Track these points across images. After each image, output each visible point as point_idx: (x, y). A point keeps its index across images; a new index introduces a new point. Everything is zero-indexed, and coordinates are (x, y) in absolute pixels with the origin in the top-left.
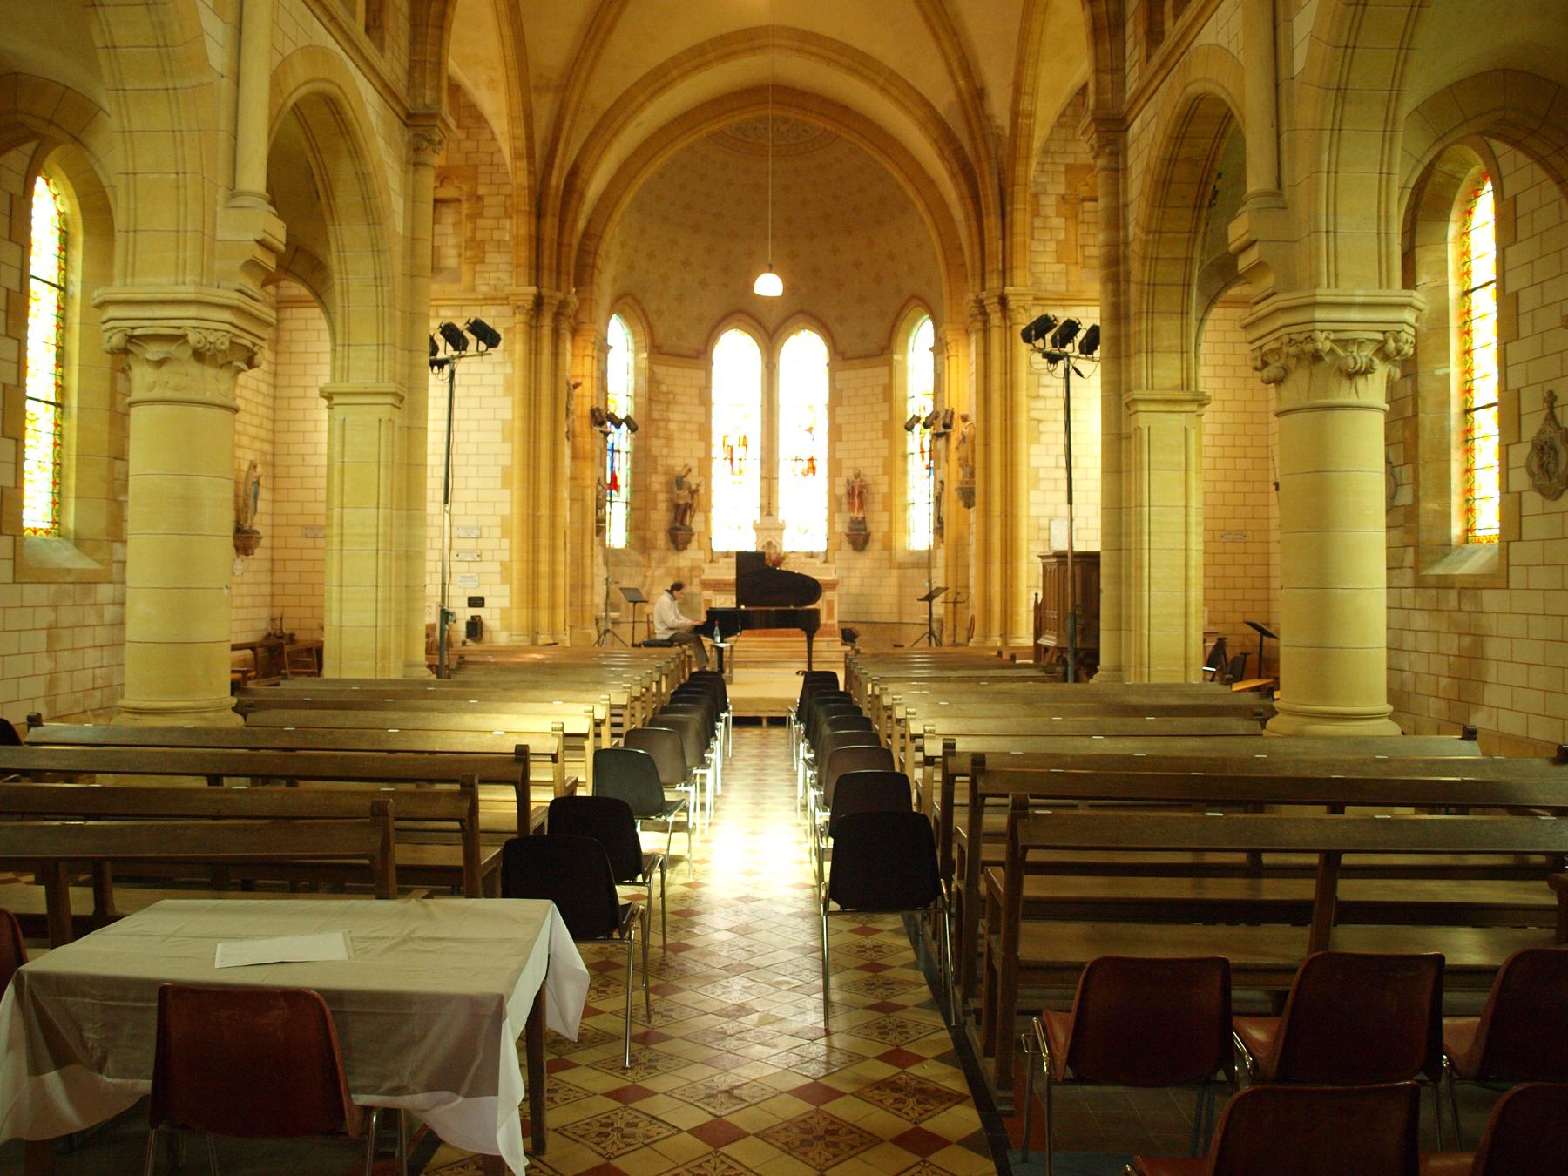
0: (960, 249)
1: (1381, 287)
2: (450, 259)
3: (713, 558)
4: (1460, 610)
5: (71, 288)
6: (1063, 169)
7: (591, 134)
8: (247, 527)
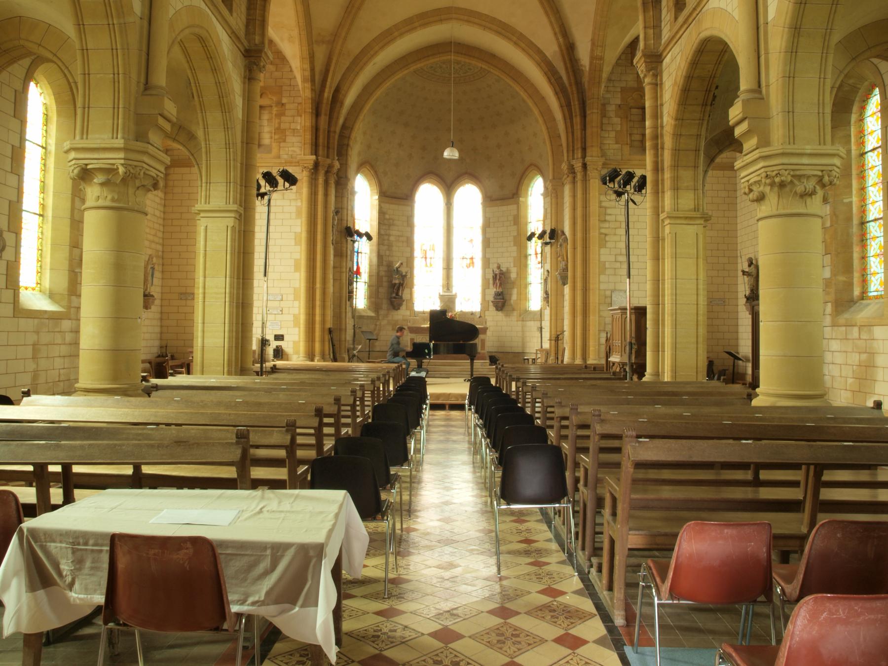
0: (559, 136)
1: (820, 144)
2: (266, 140)
3: (416, 314)
4: (860, 339)
5: (49, 148)
6: (619, 90)
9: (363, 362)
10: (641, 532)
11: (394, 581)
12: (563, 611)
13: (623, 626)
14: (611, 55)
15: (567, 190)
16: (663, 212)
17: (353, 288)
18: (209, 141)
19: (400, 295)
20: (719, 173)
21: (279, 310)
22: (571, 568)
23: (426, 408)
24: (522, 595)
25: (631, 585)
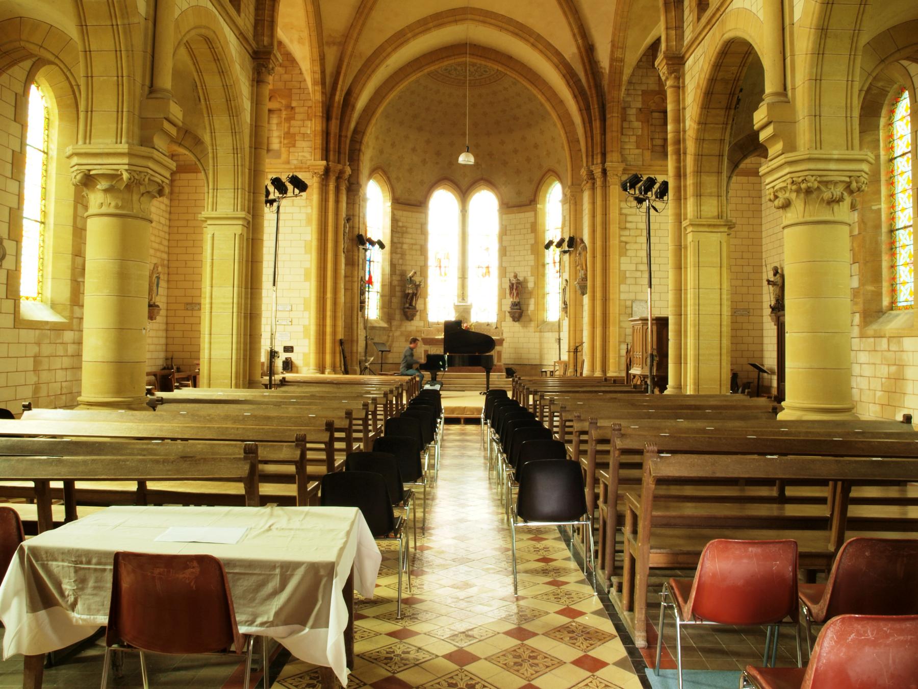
0: (578, 141)
1: (847, 149)
2: (275, 144)
4: (889, 350)
5: (50, 153)
6: (640, 93)
7: (359, 70)
10: (662, 551)
11: (407, 601)
12: (582, 632)
13: (644, 648)
14: (632, 58)
15: (586, 196)
16: (685, 219)
20: (744, 179)
21: (288, 321)
22: (590, 587)
24: (540, 616)
25: (652, 605)
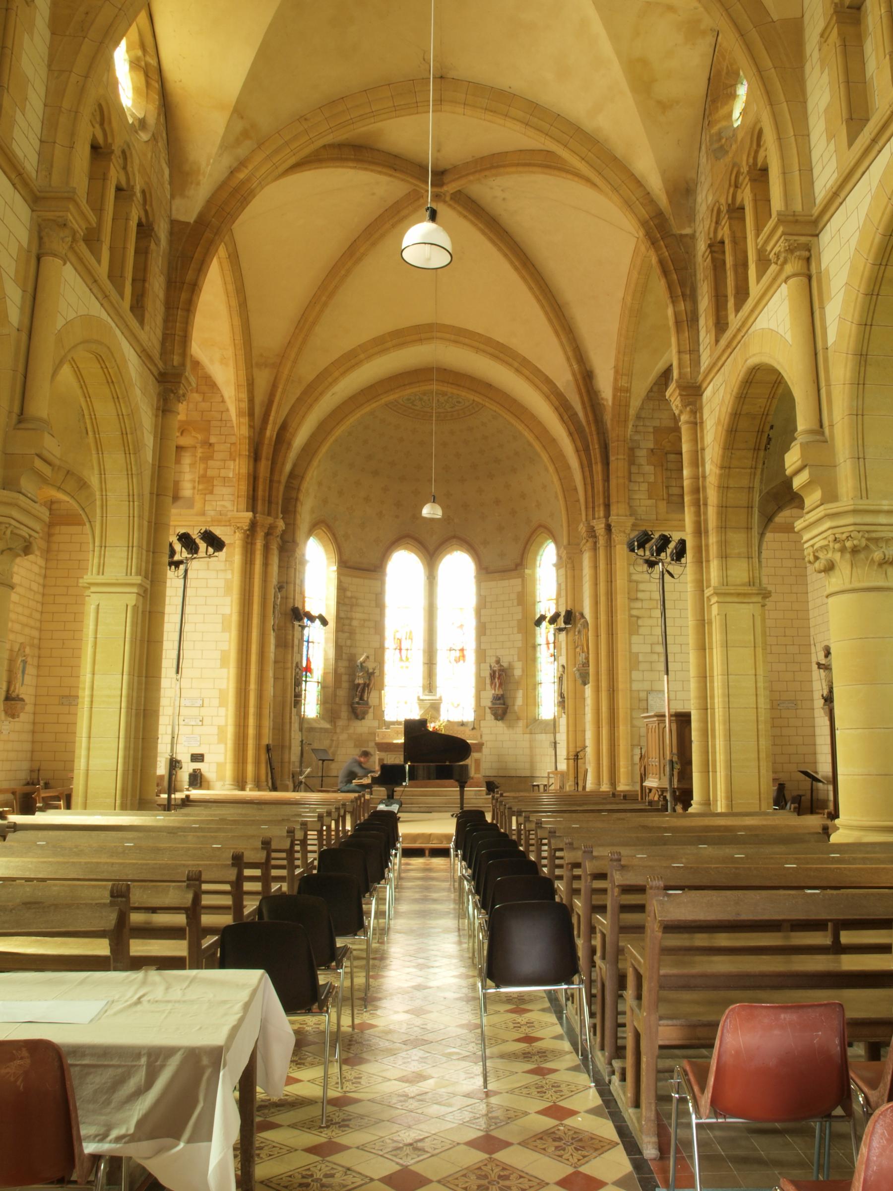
0: (576, 489)
2: (187, 490)
3: (388, 725)
6: (651, 430)
8: (14, 695)
9: (313, 792)
10: (675, 1022)
11: (336, 1102)
12: (573, 1138)
13: (655, 1159)
14: (640, 387)
15: (586, 560)
16: (708, 587)
17: (301, 691)
18: (106, 491)
19: (366, 699)
20: (780, 536)
21: (198, 720)
22: (586, 1076)
23: (396, 854)
24: (517, 1117)
25: (663, 1099)
